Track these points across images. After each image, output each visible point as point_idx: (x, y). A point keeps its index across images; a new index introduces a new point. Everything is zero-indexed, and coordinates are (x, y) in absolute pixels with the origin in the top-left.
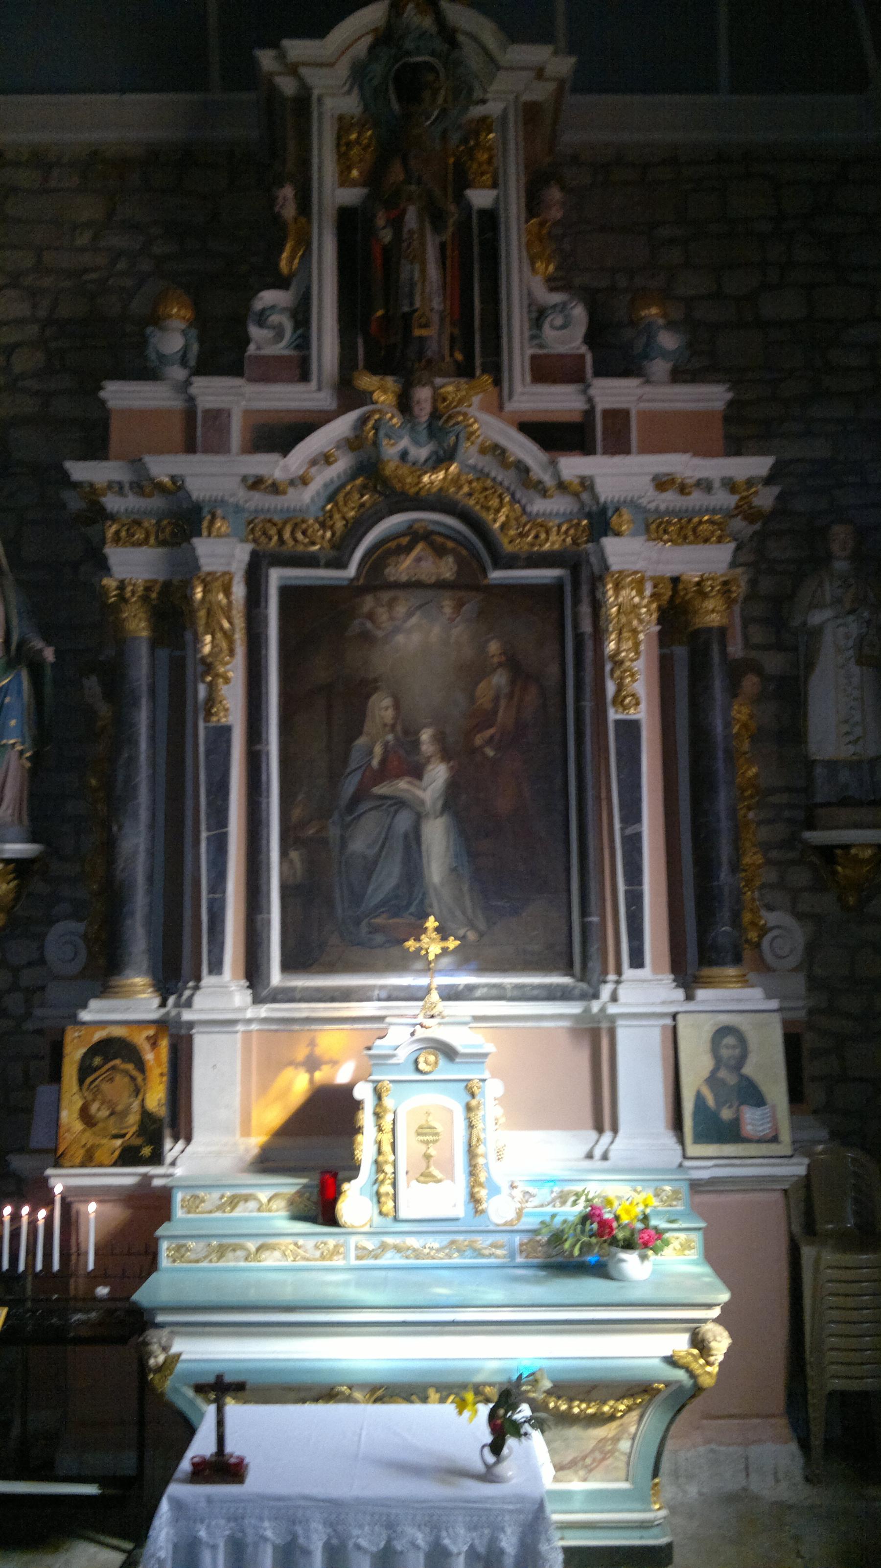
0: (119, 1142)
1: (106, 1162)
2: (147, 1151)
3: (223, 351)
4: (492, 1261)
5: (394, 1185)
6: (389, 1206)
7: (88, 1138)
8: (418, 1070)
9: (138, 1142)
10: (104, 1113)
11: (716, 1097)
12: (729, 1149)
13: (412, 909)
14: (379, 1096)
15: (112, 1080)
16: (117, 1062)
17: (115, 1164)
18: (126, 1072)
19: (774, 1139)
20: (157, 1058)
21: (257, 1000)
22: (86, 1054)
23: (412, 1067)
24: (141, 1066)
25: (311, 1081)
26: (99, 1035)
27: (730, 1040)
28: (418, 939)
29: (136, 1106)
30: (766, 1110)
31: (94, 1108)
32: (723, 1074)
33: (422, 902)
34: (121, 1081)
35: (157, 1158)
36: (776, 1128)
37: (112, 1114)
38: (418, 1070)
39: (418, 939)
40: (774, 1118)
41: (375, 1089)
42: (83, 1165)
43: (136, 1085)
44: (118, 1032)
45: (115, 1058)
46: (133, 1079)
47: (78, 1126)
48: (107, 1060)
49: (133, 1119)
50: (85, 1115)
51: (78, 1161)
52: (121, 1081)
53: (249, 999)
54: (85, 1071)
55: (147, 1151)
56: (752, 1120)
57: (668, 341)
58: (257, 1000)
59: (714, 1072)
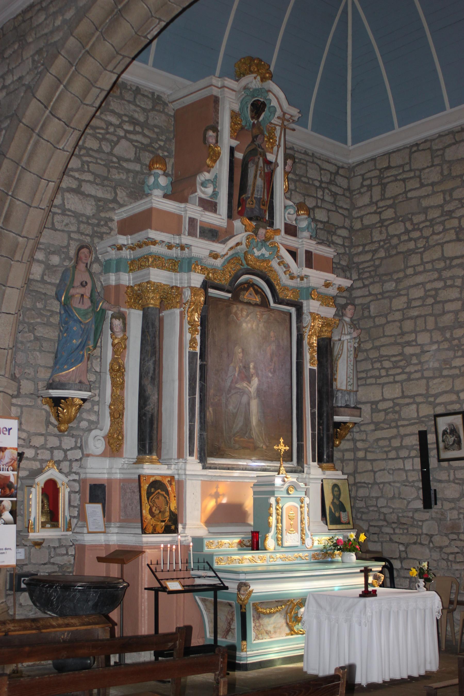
0: (164, 524)
1: (160, 532)
2: (173, 527)
3: (178, 193)
4: (305, 561)
5: (282, 535)
6: (280, 542)
7: (153, 522)
8: (288, 493)
9: (170, 523)
10: (157, 512)
11: (334, 508)
12: (338, 527)
13: (247, 435)
14: (277, 503)
15: (158, 498)
16: (159, 491)
17: (163, 533)
18: (163, 495)
19: (349, 523)
20: (172, 489)
21: (204, 468)
22: (148, 487)
23: (286, 492)
24: (167, 492)
25: (216, 502)
26: (152, 479)
27: (336, 489)
28: (278, 446)
29: (167, 509)
30: (346, 513)
31: (154, 509)
32: (335, 501)
33: (250, 433)
34: (161, 498)
35: (175, 531)
36: (349, 520)
37: (160, 512)
38: (288, 493)
39: (278, 446)
40: (348, 517)
41: (276, 500)
42: (153, 533)
43: (167, 501)
44: (158, 478)
45: (158, 489)
46: (165, 498)
47: (149, 517)
48: (156, 489)
49: (167, 514)
50: (151, 512)
51: (151, 531)
52: (161, 498)
53: (201, 467)
54: (149, 494)
55: (173, 527)
56: (344, 517)
57: (163, 181)
58: (204, 468)
59: (333, 500)
